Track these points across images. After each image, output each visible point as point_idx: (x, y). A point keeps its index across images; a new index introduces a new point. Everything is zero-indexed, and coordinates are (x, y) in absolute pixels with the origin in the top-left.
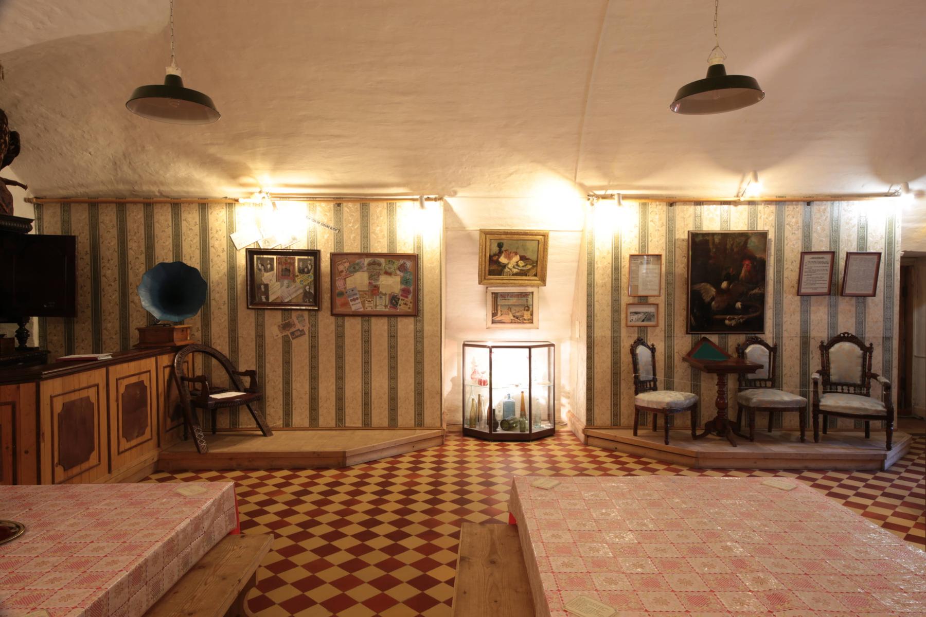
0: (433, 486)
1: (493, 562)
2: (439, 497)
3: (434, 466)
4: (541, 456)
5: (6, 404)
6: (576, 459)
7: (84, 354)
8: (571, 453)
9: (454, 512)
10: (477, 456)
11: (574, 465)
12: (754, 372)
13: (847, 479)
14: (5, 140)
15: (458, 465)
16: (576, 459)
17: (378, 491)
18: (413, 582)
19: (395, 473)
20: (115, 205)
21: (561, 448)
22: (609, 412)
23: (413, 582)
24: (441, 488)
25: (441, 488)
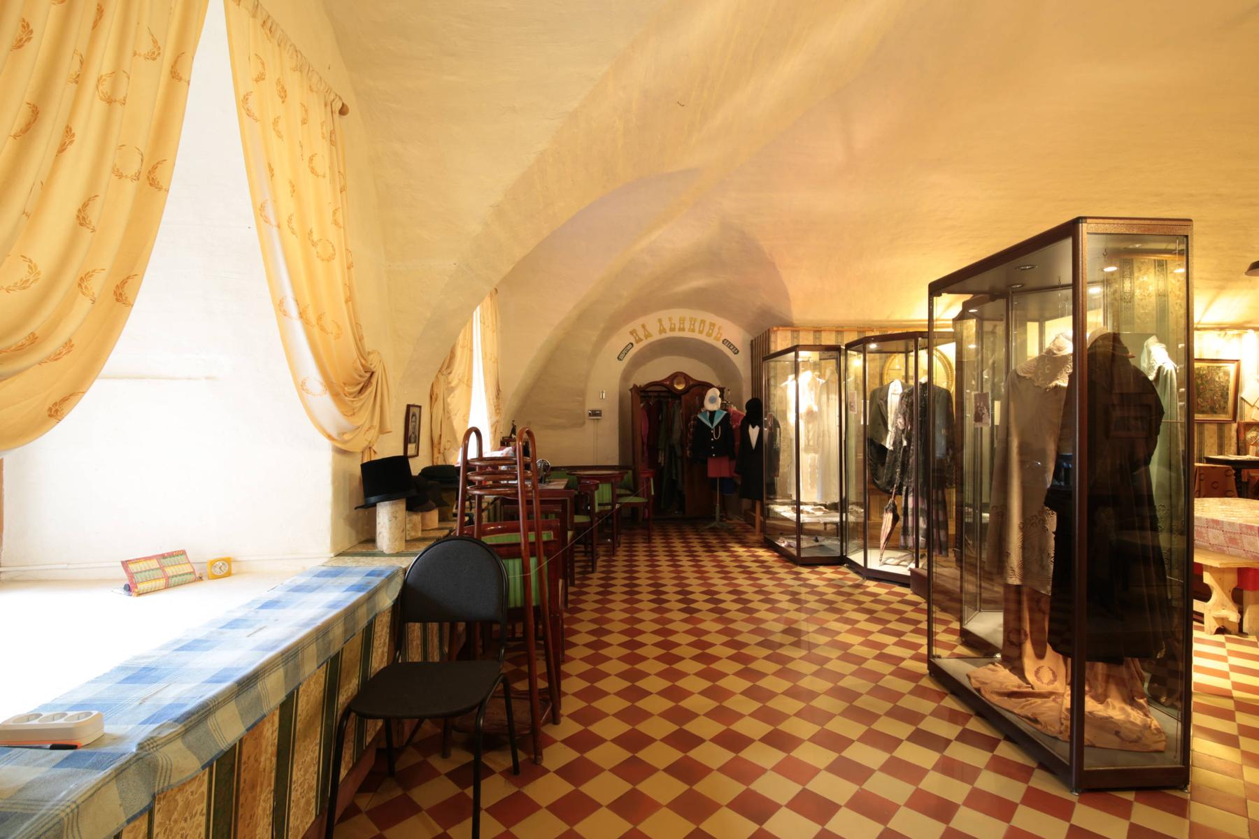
0: (636, 618)
1: (201, 578)
2: (605, 627)
3: (602, 582)
4: (724, 585)
6: (762, 597)
7: (459, 484)
8: (723, 575)
9: (623, 659)
10: (625, 572)
11: (754, 615)
13: (896, 620)
15: (627, 589)
16: (762, 597)
17: (579, 612)
18: (620, 741)
19: (585, 589)
20: (1216, 425)
21: (712, 559)
22: (1216, 435)
23: (620, 741)
24: (609, 606)
25: (609, 606)
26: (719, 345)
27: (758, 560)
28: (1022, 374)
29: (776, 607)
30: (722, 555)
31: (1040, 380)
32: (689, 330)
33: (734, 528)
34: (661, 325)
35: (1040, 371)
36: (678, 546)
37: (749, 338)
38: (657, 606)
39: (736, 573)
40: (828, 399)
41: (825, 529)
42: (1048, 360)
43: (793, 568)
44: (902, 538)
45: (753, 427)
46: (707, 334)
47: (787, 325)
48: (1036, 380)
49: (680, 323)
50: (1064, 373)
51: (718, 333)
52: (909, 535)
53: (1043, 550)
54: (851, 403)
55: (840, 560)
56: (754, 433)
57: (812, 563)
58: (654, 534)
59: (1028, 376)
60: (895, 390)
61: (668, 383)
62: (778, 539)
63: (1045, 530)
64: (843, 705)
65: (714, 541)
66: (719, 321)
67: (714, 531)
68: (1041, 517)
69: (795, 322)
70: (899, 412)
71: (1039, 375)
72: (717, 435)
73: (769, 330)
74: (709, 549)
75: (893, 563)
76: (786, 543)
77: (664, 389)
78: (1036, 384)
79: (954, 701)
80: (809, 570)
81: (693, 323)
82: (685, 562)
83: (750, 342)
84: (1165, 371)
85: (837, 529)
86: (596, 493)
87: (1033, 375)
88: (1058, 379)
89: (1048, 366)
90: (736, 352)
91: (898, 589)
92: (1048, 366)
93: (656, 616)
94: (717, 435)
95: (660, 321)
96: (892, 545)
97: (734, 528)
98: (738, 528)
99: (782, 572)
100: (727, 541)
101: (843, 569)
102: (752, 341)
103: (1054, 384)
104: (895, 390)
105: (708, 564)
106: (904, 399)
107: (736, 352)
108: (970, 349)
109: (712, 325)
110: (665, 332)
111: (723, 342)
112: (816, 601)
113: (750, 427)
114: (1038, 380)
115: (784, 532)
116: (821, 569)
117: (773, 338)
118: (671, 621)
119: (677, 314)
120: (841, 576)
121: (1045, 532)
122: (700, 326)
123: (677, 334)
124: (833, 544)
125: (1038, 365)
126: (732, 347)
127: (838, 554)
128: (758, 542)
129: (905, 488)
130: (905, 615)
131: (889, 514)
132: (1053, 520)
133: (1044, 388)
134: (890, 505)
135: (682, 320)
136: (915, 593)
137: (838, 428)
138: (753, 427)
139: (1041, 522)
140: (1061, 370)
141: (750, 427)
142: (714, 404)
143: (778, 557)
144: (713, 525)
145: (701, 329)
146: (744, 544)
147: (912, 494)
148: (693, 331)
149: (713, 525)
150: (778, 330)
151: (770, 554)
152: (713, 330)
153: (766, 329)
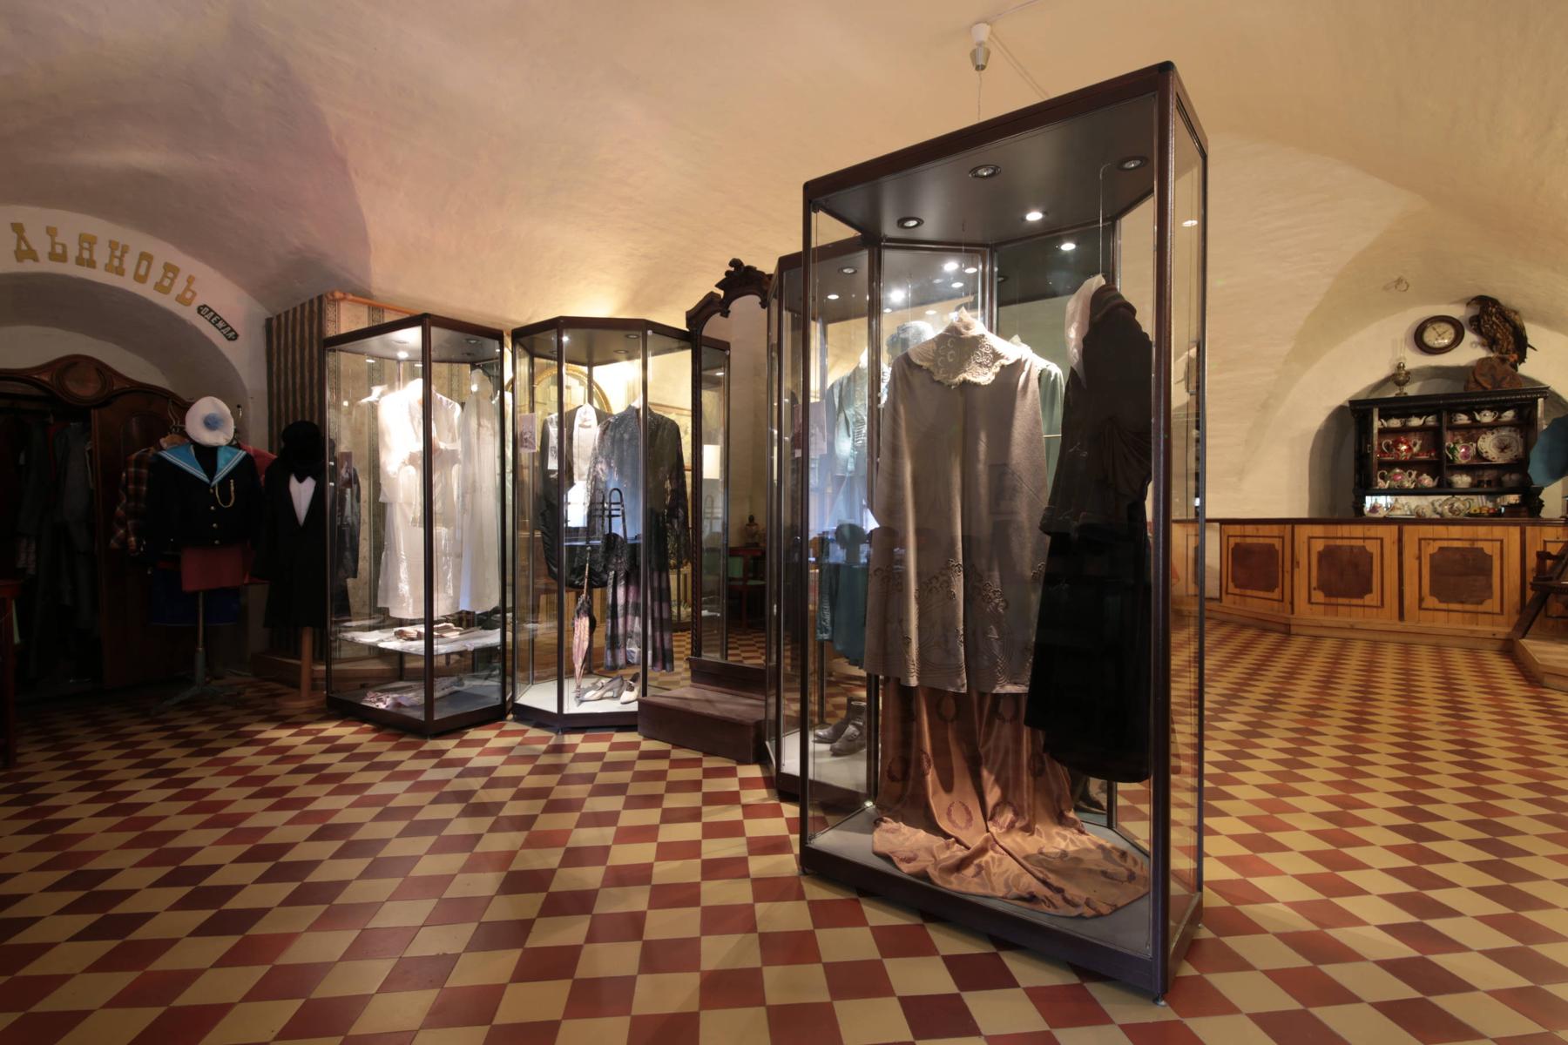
5: (1377, 538)
12: (1491, 557)
14: (1494, 322)
26: (189, 314)
27: (334, 746)
28: (918, 362)
29: (1547, 994)
30: (246, 755)
31: (941, 372)
32: (108, 268)
33: (239, 694)
34: (21, 238)
35: (940, 359)
36: (106, 757)
37: (262, 313)
38: (112, 944)
39: (302, 786)
40: (479, 425)
41: (448, 663)
42: (952, 343)
43: (421, 745)
44: (609, 653)
45: (301, 480)
46: (157, 284)
47: (362, 295)
48: (936, 373)
49: (81, 248)
50: (973, 362)
51: (188, 289)
52: (619, 648)
53: (949, 625)
54: (521, 435)
55: (493, 716)
56: (302, 492)
57: (454, 728)
58: (19, 750)
59: (925, 364)
60: (585, 421)
61: (46, 378)
62: (365, 695)
63: (952, 596)
64: (586, 969)
65: (206, 729)
66: (188, 265)
67: (194, 706)
68: (945, 578)
69: (375, 293)
70: (601, 453)
71: (940, 364)
72: (226, 499)
73: (320, 298)
74: (201, 748)
75: (595, 697)
76: (389, 701)
77: (35, 391)
78: (937, 378)
79: (874, 908)
80: (455, 742)
81: (118, 253)
82: (148, 793)
83: (263, 322)
84: (1053, 375)
85: (625, 645)
86: (477, 612)
87: (932, 364)
88: (965, 371)
89: (952, 352)
90: (232, 336)
91: (620, 737)
92: (952, 352)
93: (123, 980)
94: (226, 499)
95: (18, 228)
96: (593, 666)
97: (239, 694)
98: (249, 693)
99: (406, 760)
100: (235, 721)
101: (510, 725)
102: (269, 321)
103: (961, 377)
104: (585, 421)
105: (222, 787)
106: (608, 432)
107: (232, 336)
108: (1067, 254)
109: (170, 269)
110: (36, 259)
111: (199, 310)
112: (408, 790)
113: (294, 482)
114: (938, 372)
115: (380, 682)
116: (473, 734)
117: (330, 313)
118: (188, 977)
119: (72, 225)
120: (519, 739)
121: (951, 599)
122: (138, 266)
123: (70, 269)
124: (486, 687)
125: (938, 349)
126: (220, 324)
127: (495, 699)
128: (311, 711)
129: (612, 573)
130: (470, 765)
131: (584, 618)
132: (959, 580)
133: (947, 384)
134: (582, 604)
135: (87, 241)
136: (648, 737)
137: (498, 478)
138: (301, 480)
139: (946, 585)
140: (969, 358)
141: (294, 482)
142: (217, 432)
143: (374, 731)
144: (188, 694)
145: (142, 271)
146: (284, 722)
147: (623, 582)
148: (120, 271)
149: (188, 694)
150: (343, 299)
151: (353, 729)
152: (172, 280)
153: (315, 296)
